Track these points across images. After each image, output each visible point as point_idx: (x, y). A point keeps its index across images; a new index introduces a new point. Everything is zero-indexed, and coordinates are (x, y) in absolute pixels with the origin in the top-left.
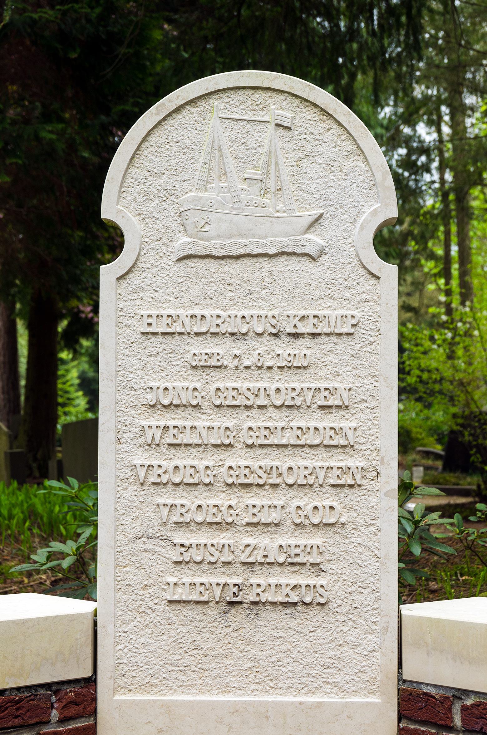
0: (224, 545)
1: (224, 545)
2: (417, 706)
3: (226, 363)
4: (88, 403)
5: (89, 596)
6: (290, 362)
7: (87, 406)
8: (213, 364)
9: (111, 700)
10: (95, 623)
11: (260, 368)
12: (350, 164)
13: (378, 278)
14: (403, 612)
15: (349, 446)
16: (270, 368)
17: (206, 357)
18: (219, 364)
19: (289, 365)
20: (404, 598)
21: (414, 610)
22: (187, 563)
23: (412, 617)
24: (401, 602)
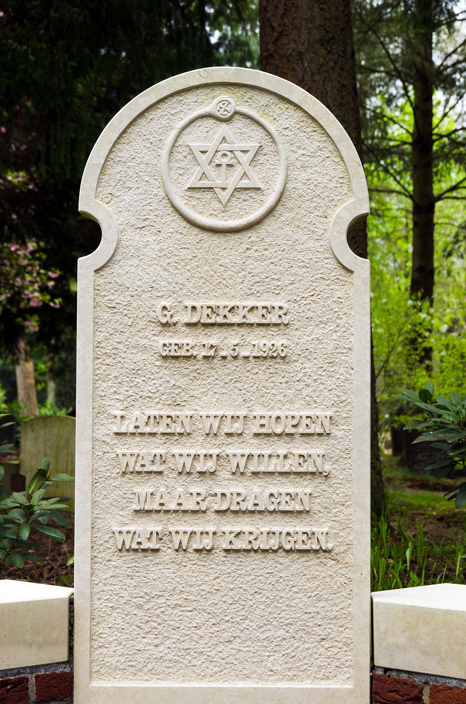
0: (152, 533)
1: (152, 533)
3: (195, 353)
4: (6, 395)
5: (69, 583)
6: (265, 352)
7: (4, 398)
8: (183, 354)
9: (92, 690)
10: (71, 611)
11: (235, 358)
12: (340, 163)
13: (352, 272)
14: (375, 600)
15: (325, 434)
16: (246, 358)
17: (176, 347)
18: (188, 354)
19: (265, 355)
20: (64, 579)
21: (385, 598)
22: (275, 551)
23: (386, 605)
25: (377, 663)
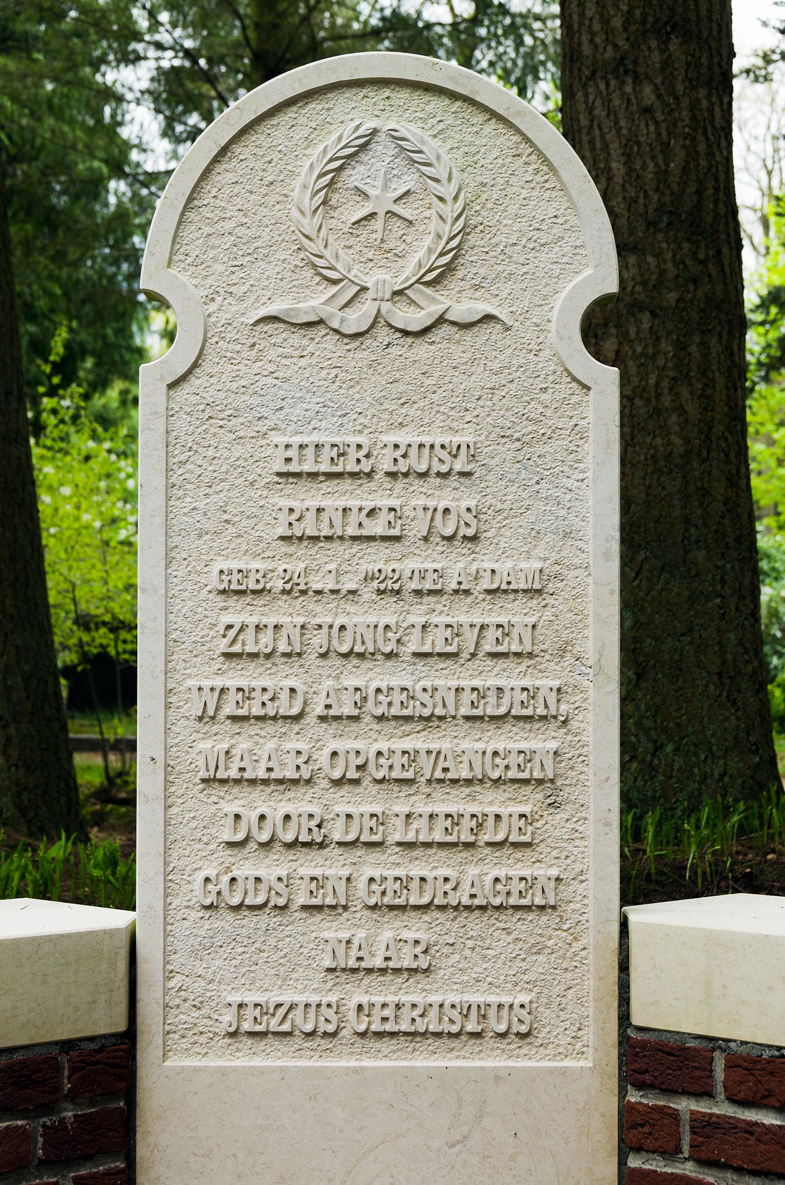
2: (654, 1062)
24: (644, 882)
25: (638, 1018)
